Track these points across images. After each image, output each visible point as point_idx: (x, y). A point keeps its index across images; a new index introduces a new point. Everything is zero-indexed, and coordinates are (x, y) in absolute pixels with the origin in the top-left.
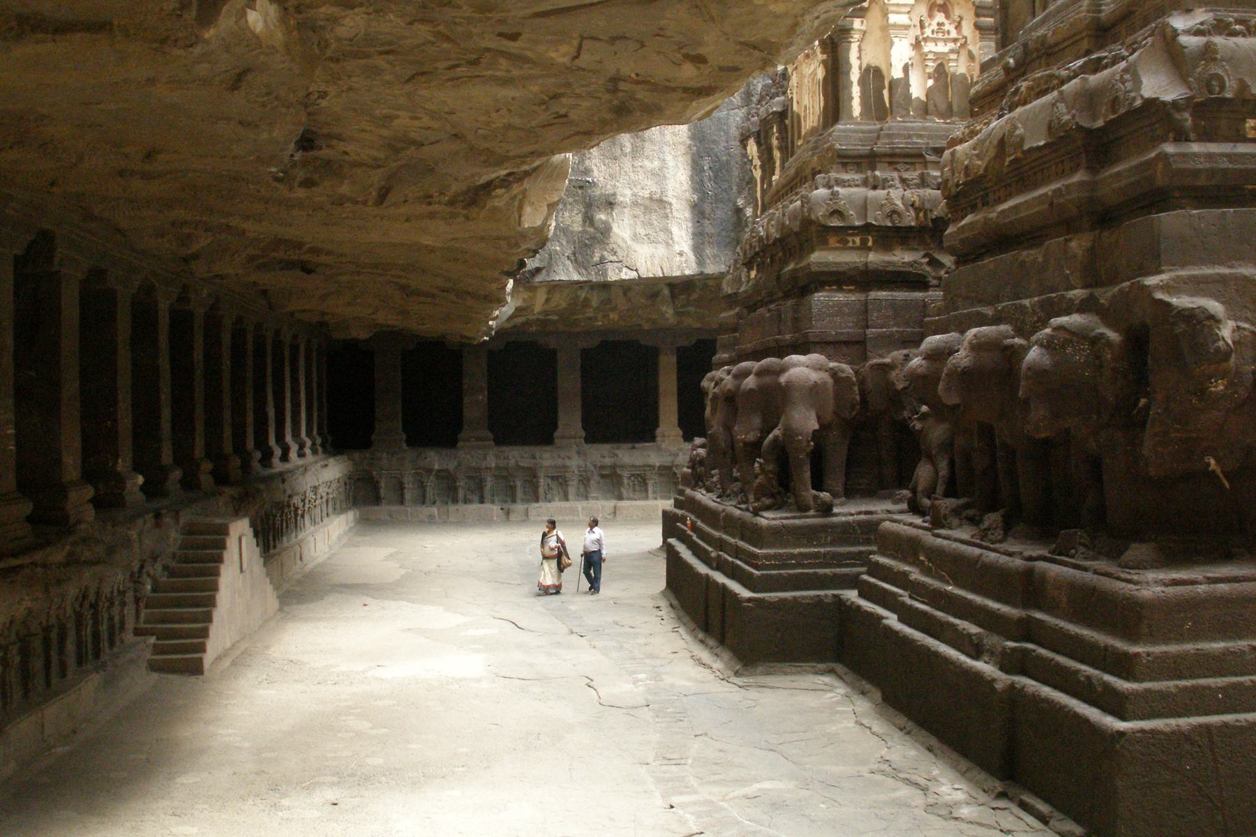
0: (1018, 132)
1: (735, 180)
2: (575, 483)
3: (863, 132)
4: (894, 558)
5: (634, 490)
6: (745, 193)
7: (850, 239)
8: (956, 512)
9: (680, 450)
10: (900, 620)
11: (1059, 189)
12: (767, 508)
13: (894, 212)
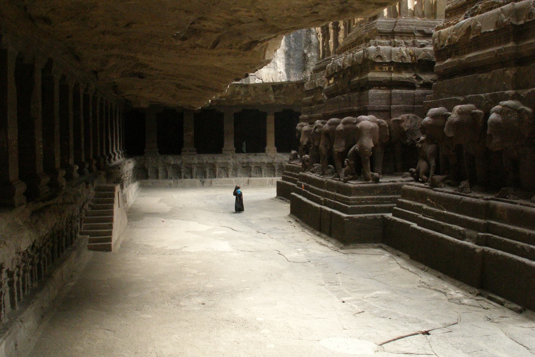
0: (478, 25)
1: (304, 42)
2: (231, 170)
3: (388, 23)
4: (411, 200)
5: (256, 173)
6: (308, 47)
7: (384, 67)
8: (443, 181)
9: (276, 156)
10: (418, 225)
11: (501, 49)
12: (351, 180)
13: (403, 57)
